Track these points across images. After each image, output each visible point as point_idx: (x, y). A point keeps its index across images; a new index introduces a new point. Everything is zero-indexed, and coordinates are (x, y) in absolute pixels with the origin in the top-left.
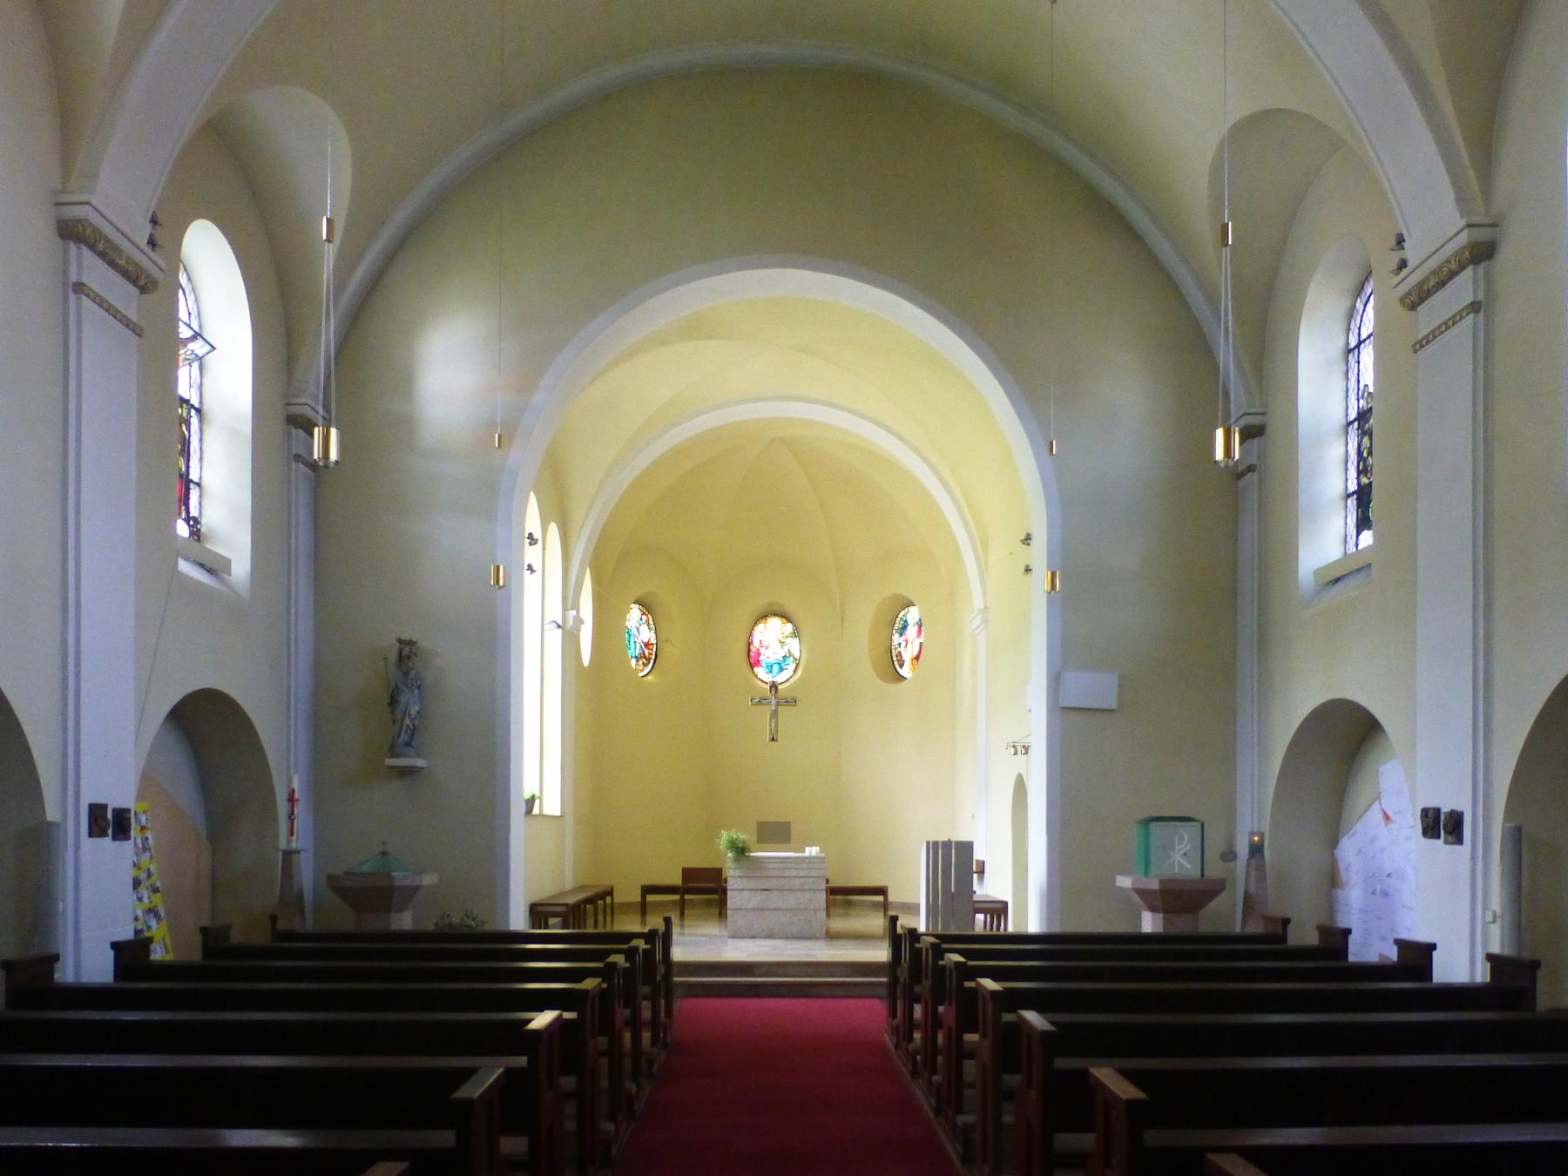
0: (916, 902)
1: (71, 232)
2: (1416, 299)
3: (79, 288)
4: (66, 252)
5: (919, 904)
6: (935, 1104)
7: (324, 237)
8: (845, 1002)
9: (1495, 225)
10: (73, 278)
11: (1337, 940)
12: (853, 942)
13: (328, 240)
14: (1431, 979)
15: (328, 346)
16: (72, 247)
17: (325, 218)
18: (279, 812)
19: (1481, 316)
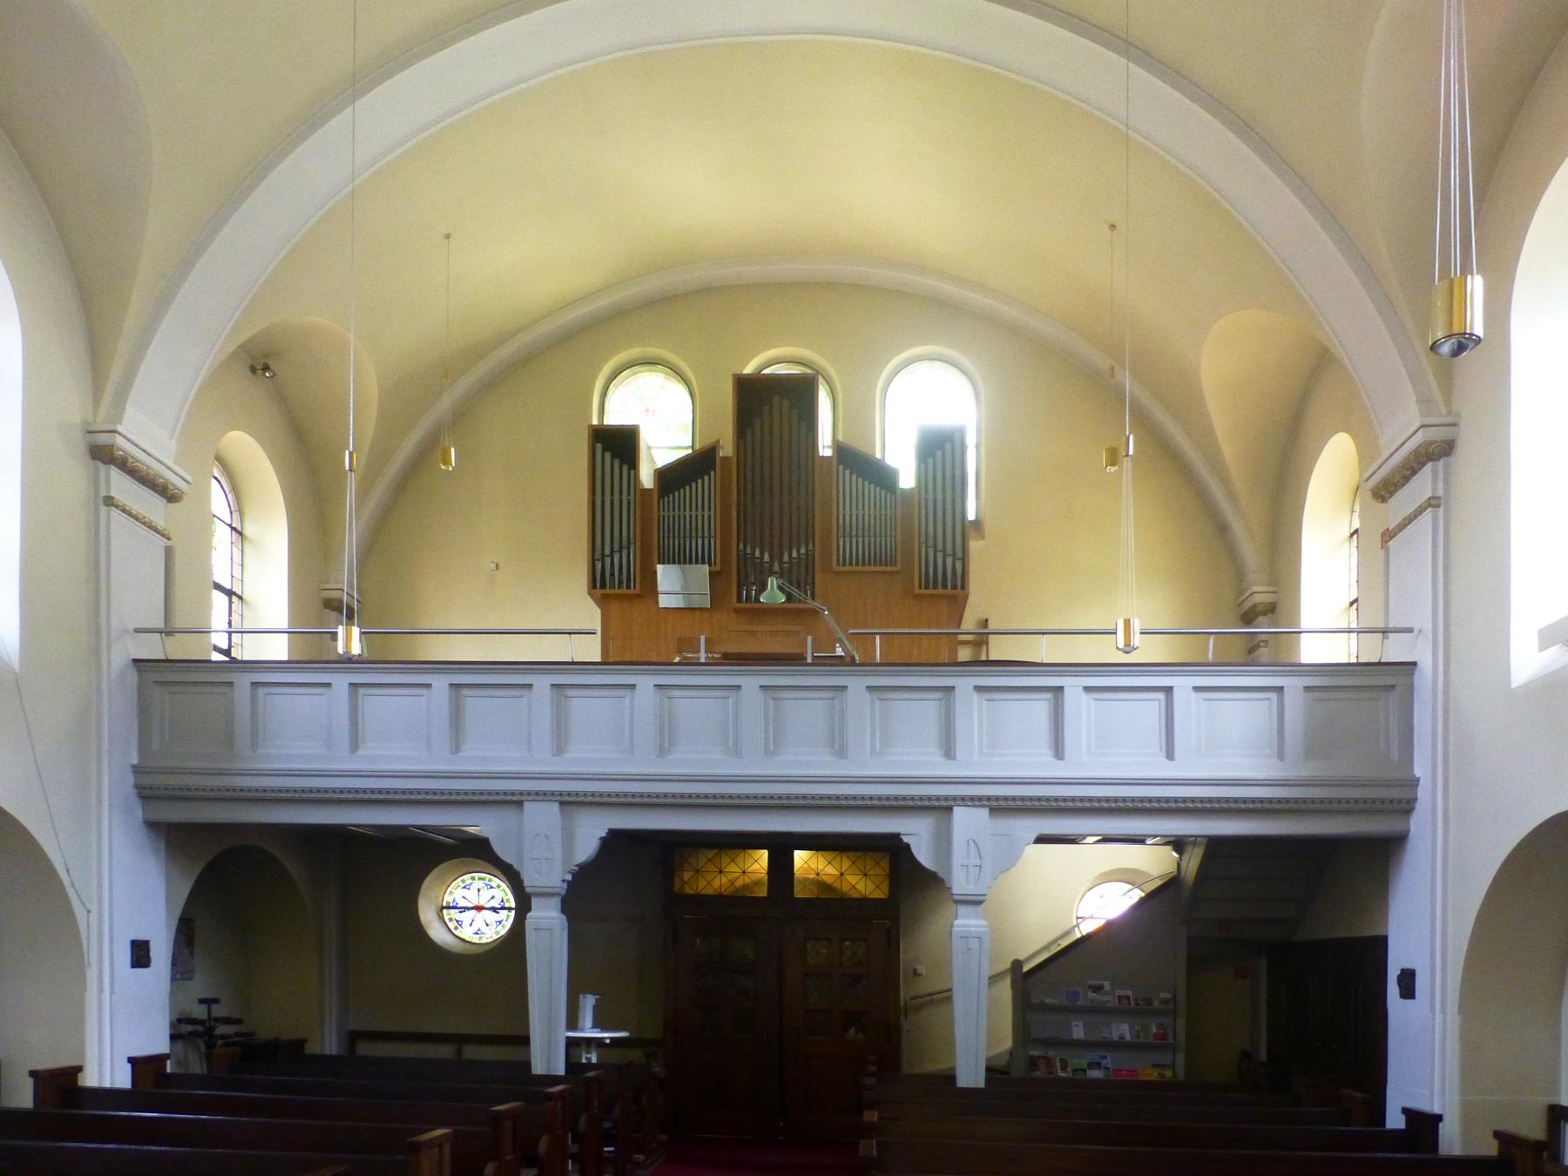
0: (1384, 934)
1: (103, 454)
2: (1384, 491)
3: (109, 501)
4: (97, 470)
5: (1387, 937)
6: (715, 851)
7: (347, 468)
8: (817, 526)
9: (1454, 425)
10: (103, 493)
11: (950, 1078)
12: (591, 580)
13: (351, 470)
14: (1384, 1126)
15: (351, 563)
16: (101, 466)
17: (347, 452)
18: (82, 936)
19: (1441, 510)
